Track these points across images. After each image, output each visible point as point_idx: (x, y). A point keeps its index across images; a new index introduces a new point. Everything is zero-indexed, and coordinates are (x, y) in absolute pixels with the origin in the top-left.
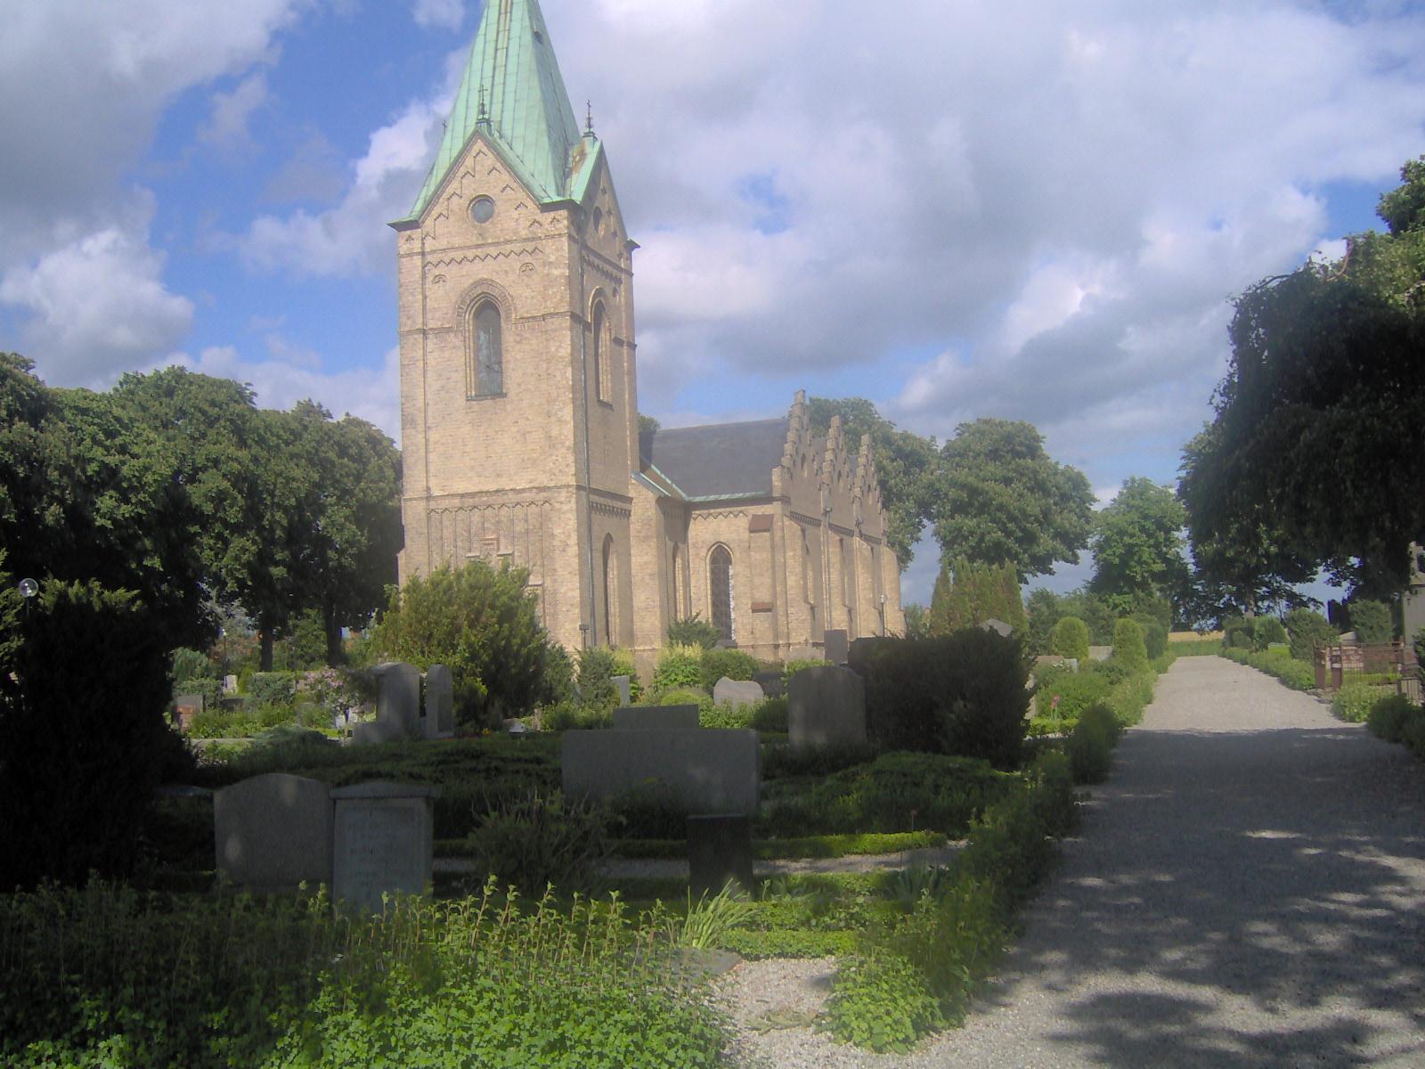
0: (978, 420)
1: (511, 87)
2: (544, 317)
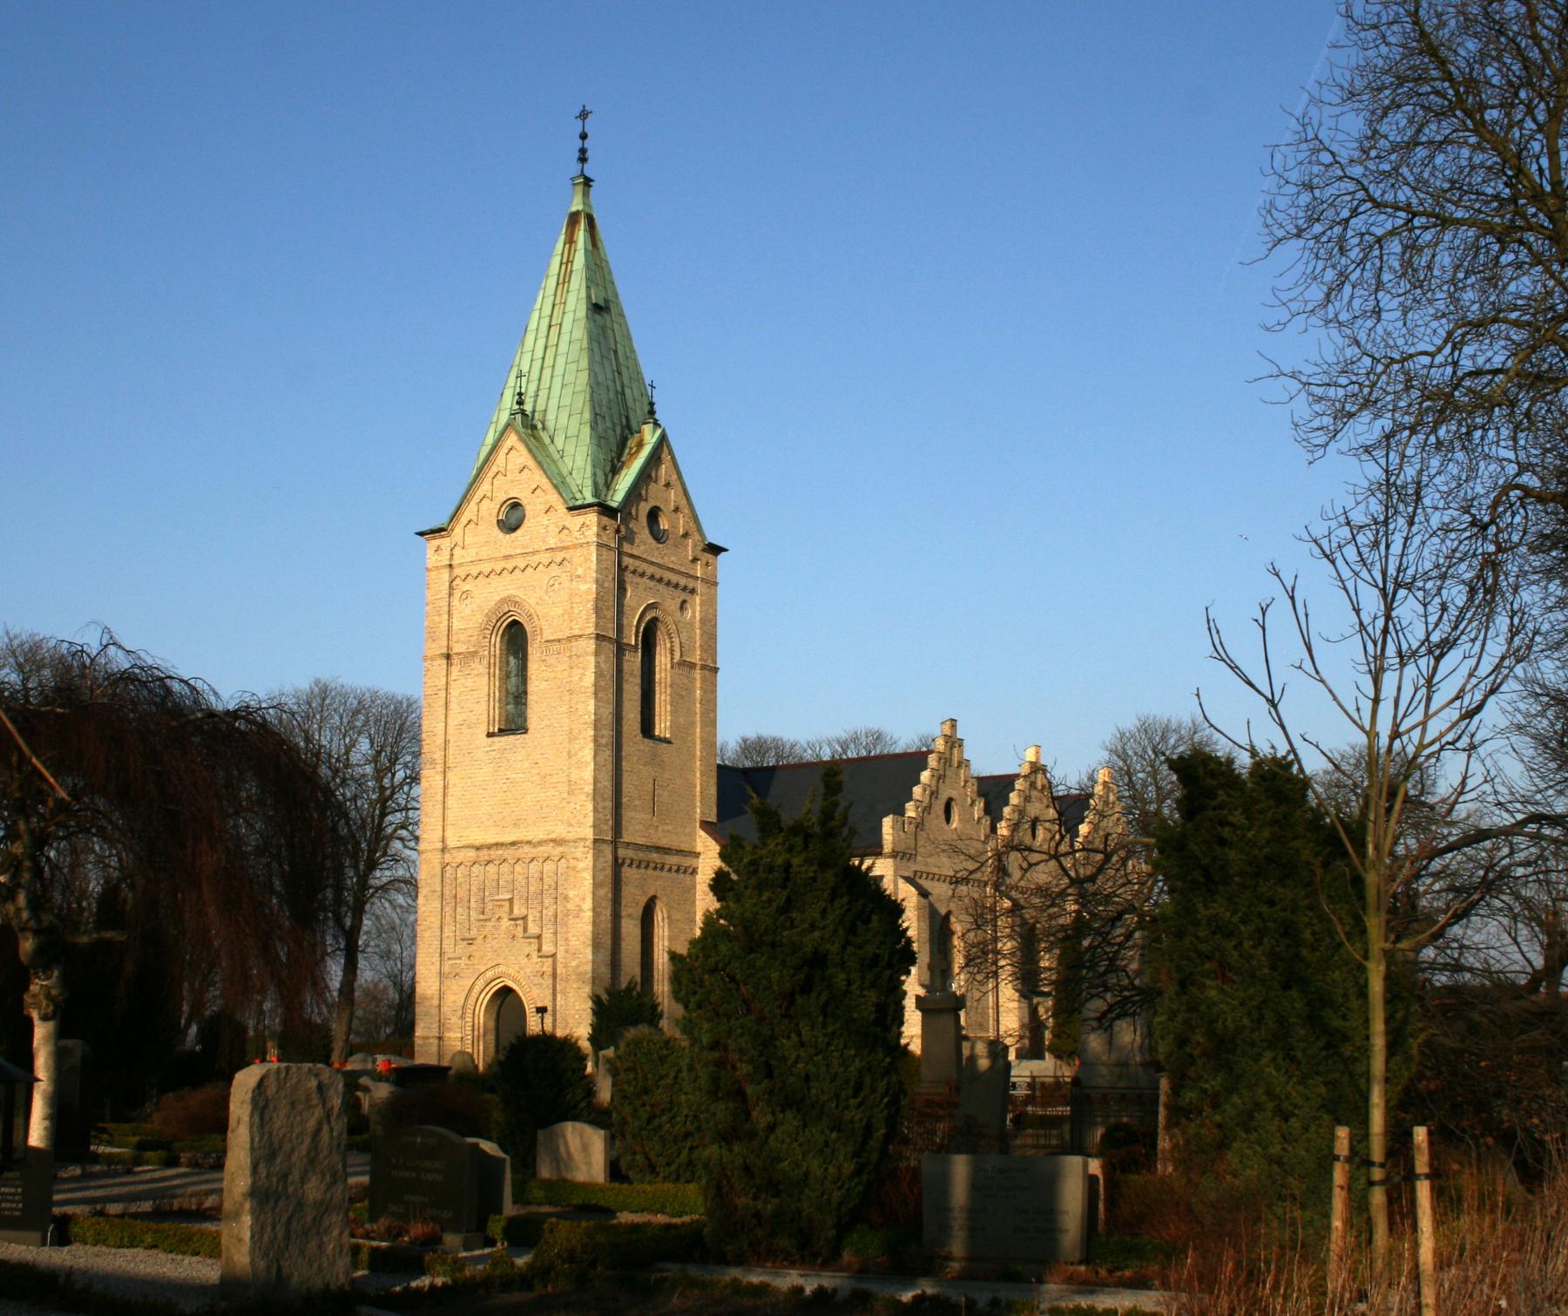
0: (1037, 768)
1: (559, 370)
2: (569, 639)
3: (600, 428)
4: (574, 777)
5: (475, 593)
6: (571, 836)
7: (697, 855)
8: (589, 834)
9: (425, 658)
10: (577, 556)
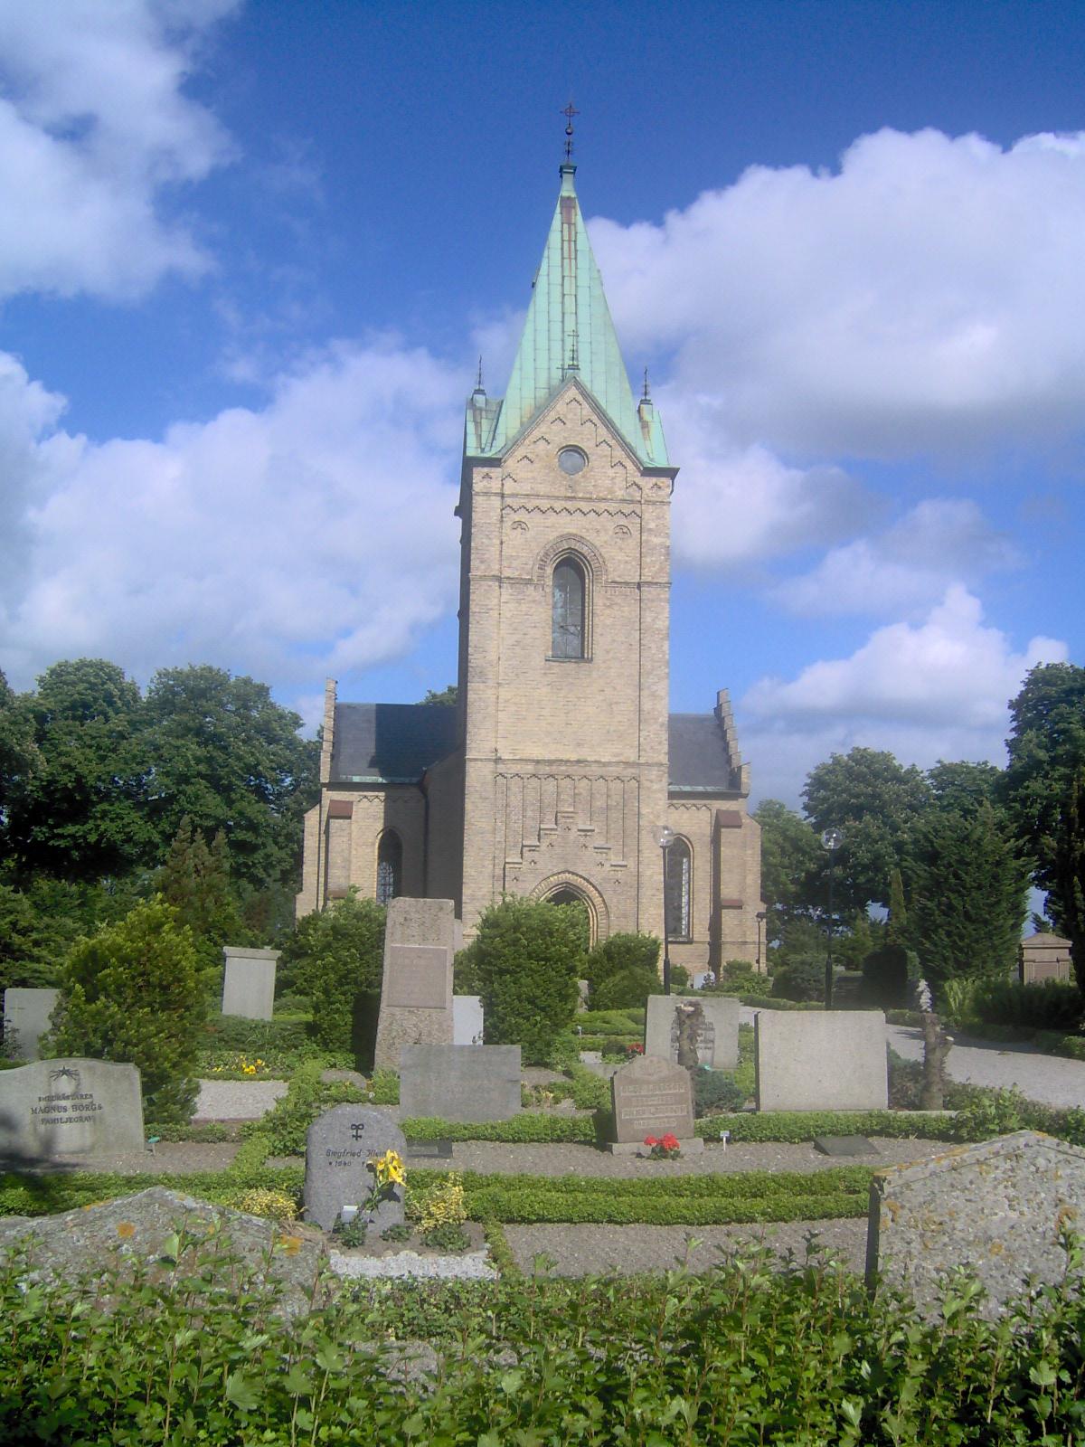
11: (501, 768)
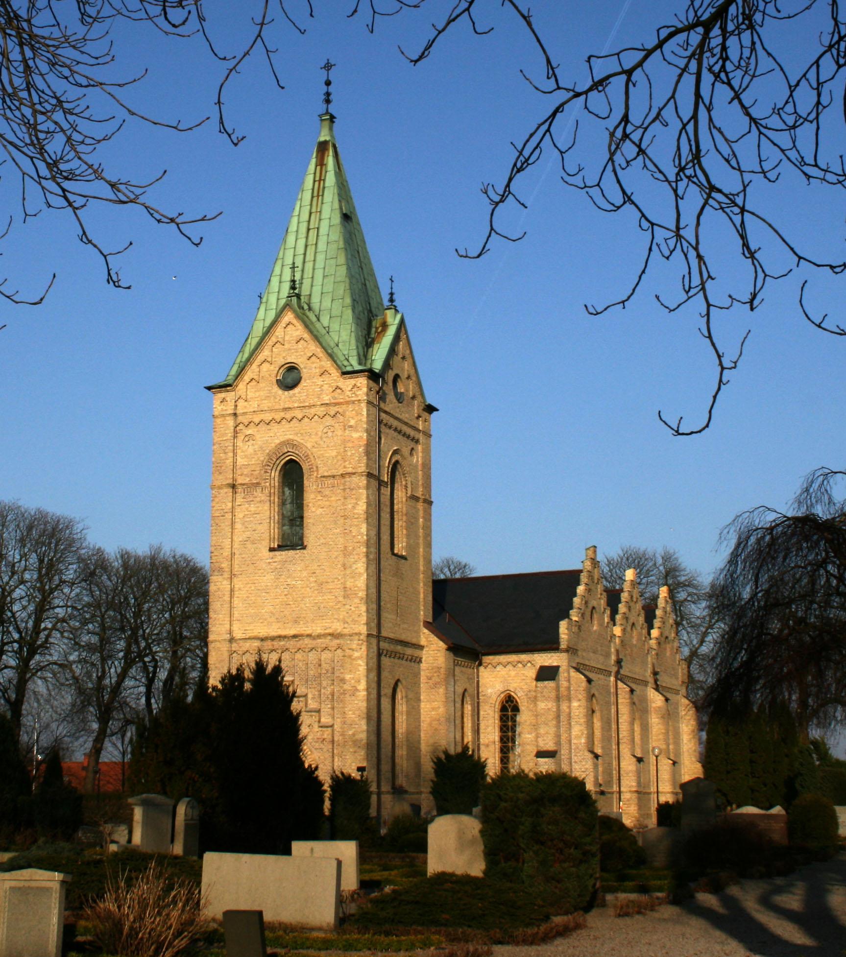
1: (320, 264)
2: (342, 476)
3: (356, 311)
4: (349, 584)
5: (258, 437)
6: (346, 631)
7: (421, 647)
8: (364, 630)
9: (213, 487)
10: (350, 410)
11: (235, 646)
